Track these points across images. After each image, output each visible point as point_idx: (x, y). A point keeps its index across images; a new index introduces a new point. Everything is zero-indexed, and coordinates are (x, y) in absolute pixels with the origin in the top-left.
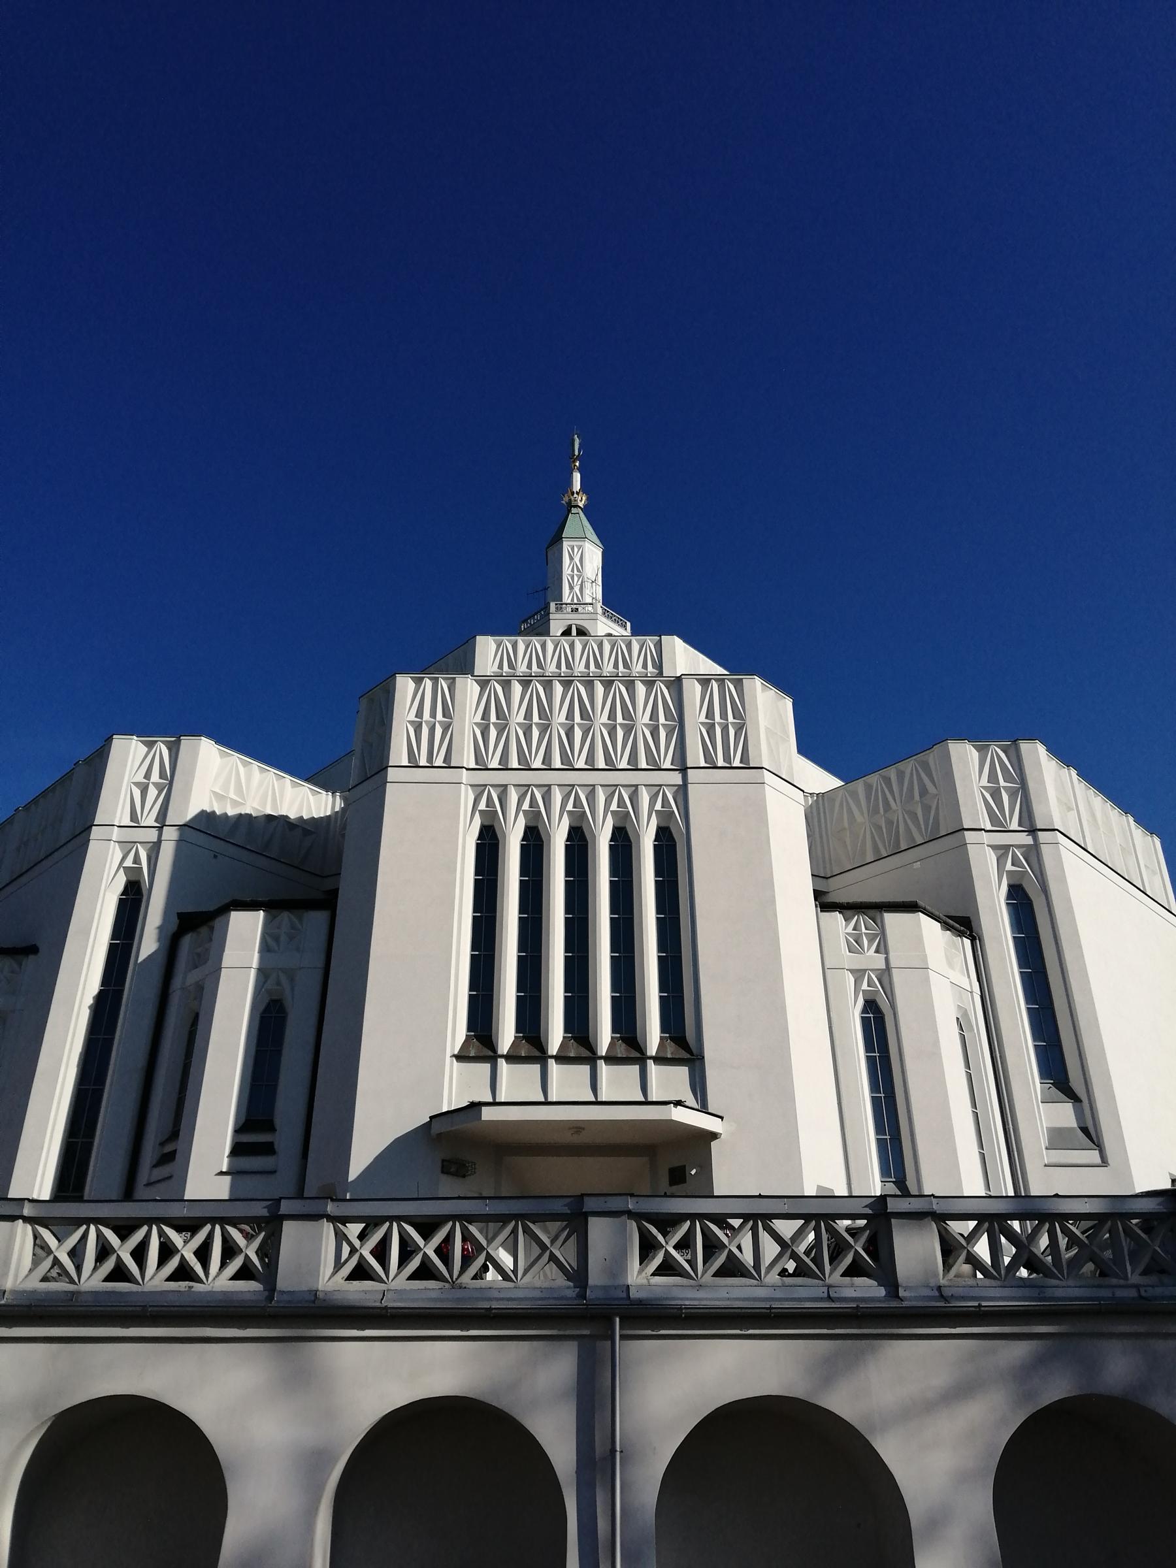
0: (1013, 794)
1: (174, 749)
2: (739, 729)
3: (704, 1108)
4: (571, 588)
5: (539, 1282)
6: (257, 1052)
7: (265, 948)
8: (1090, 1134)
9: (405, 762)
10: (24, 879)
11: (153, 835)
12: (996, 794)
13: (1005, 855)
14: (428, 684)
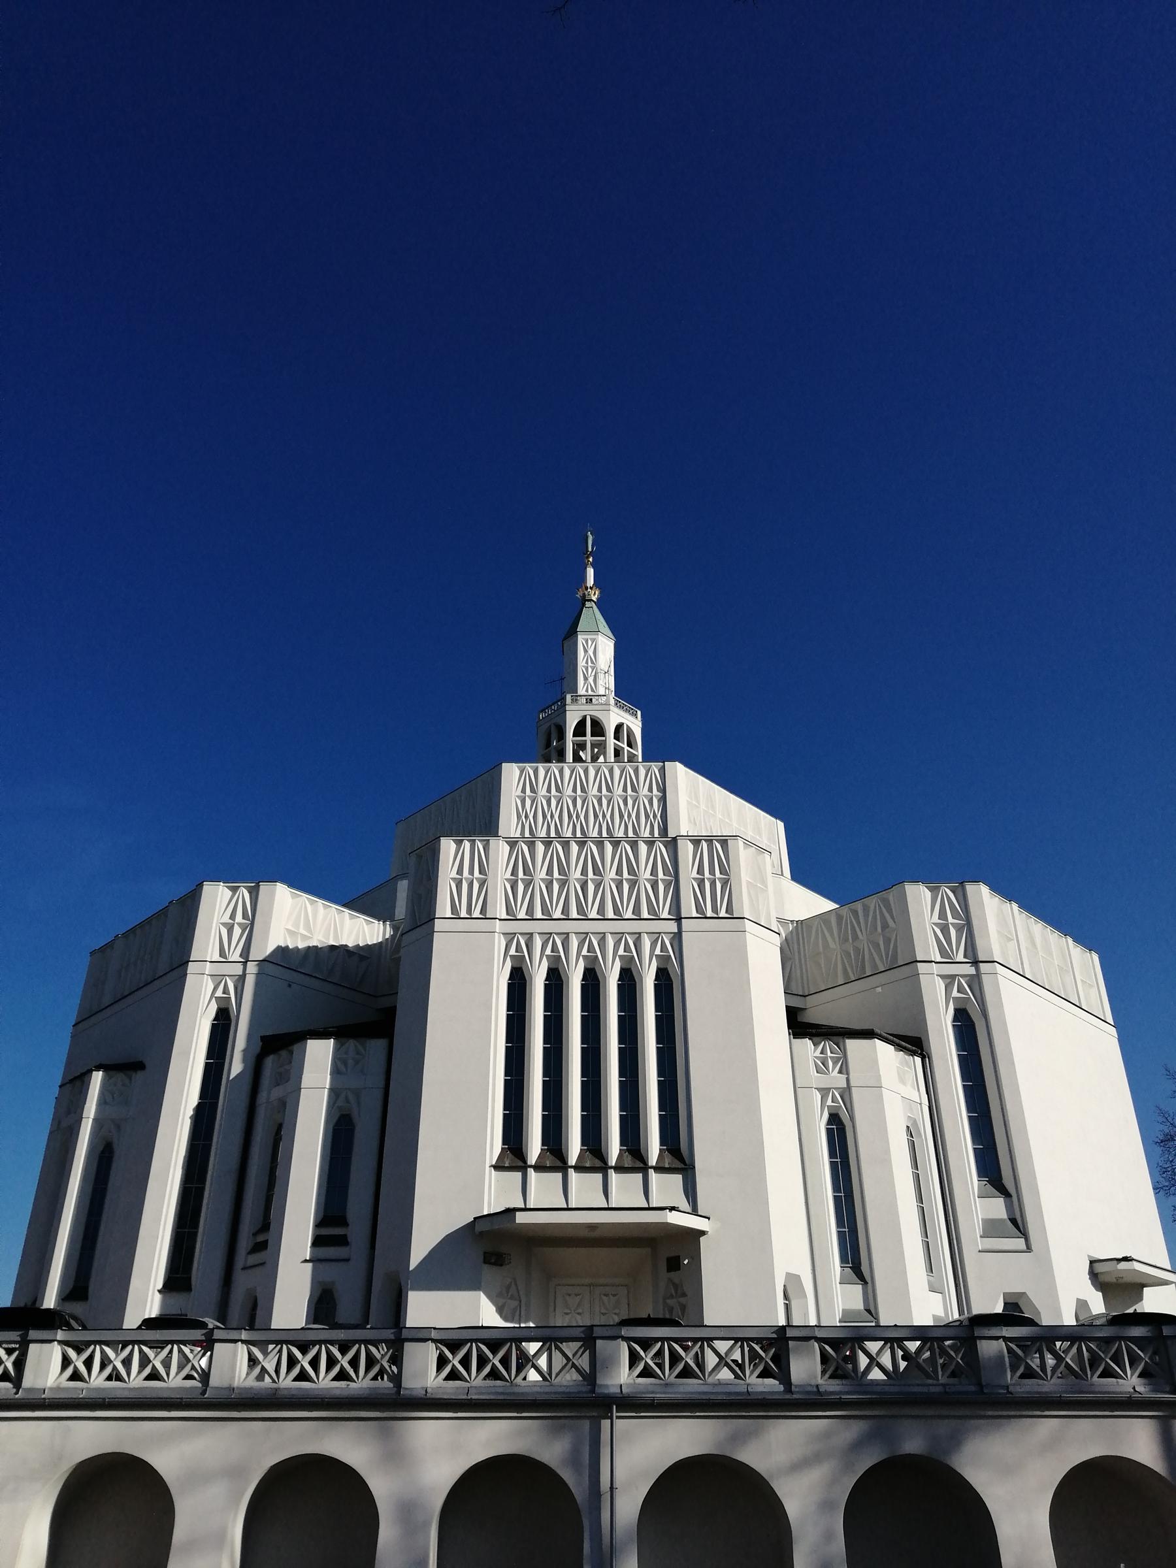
0: (959, 929)
1: (254, 893)
2: (725, 883)
3: (695, 1212)
4: (586, 679)
5: (568, 1377)
6: (332, 1159)
7: (336, 1072)
8: (1017, 1224)
9: (449, 915)
10: (130, 1000)
11: (238, 969)
12: (945, 929)
14: (467, 845)
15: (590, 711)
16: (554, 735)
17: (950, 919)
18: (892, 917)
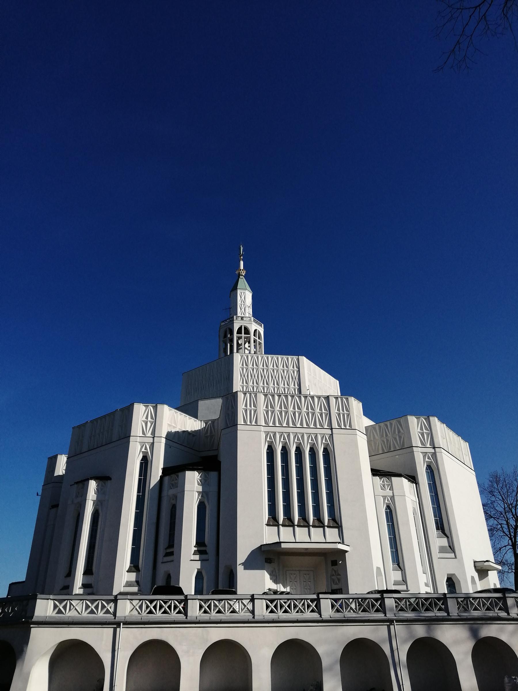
3: (343, 543)
8: (452, 548)
11: (151, 440)
12: (422, 434)
13: (425, 456)
15: (243, 323)
16: (228, 332)
17: (424, 431)
18: (402, 428)
